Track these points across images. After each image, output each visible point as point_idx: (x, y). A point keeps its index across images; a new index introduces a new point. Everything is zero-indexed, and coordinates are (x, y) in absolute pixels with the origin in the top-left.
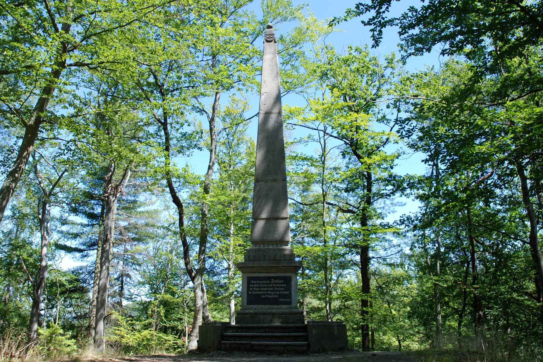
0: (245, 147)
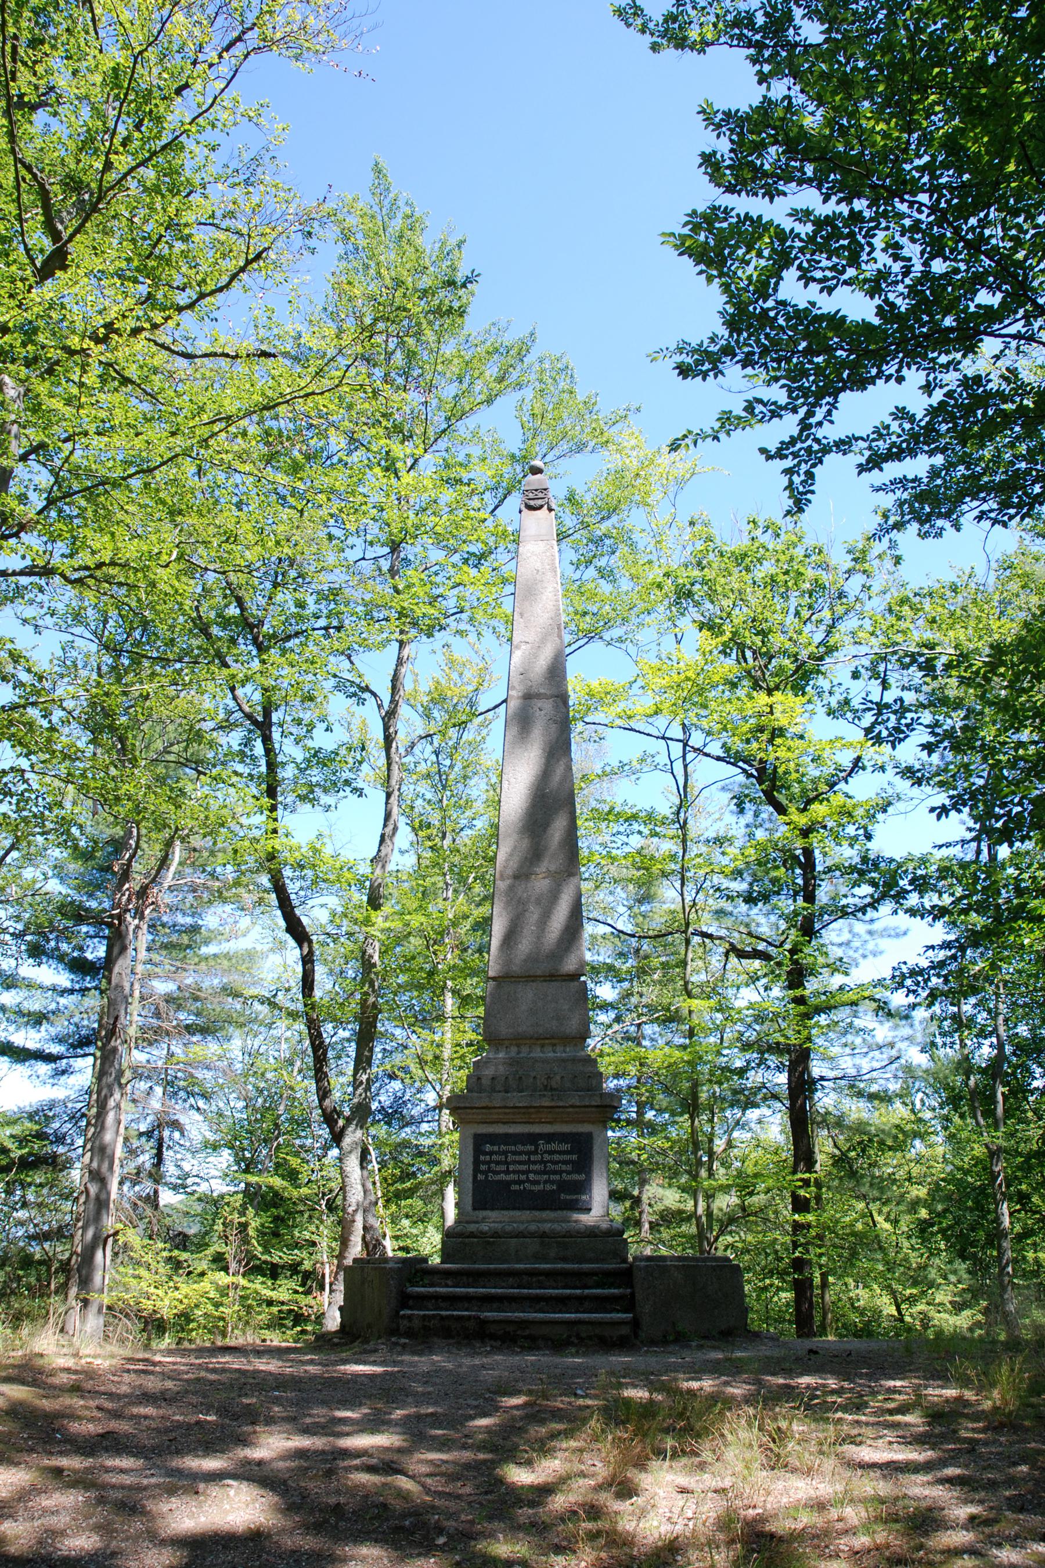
0: (483, 786)
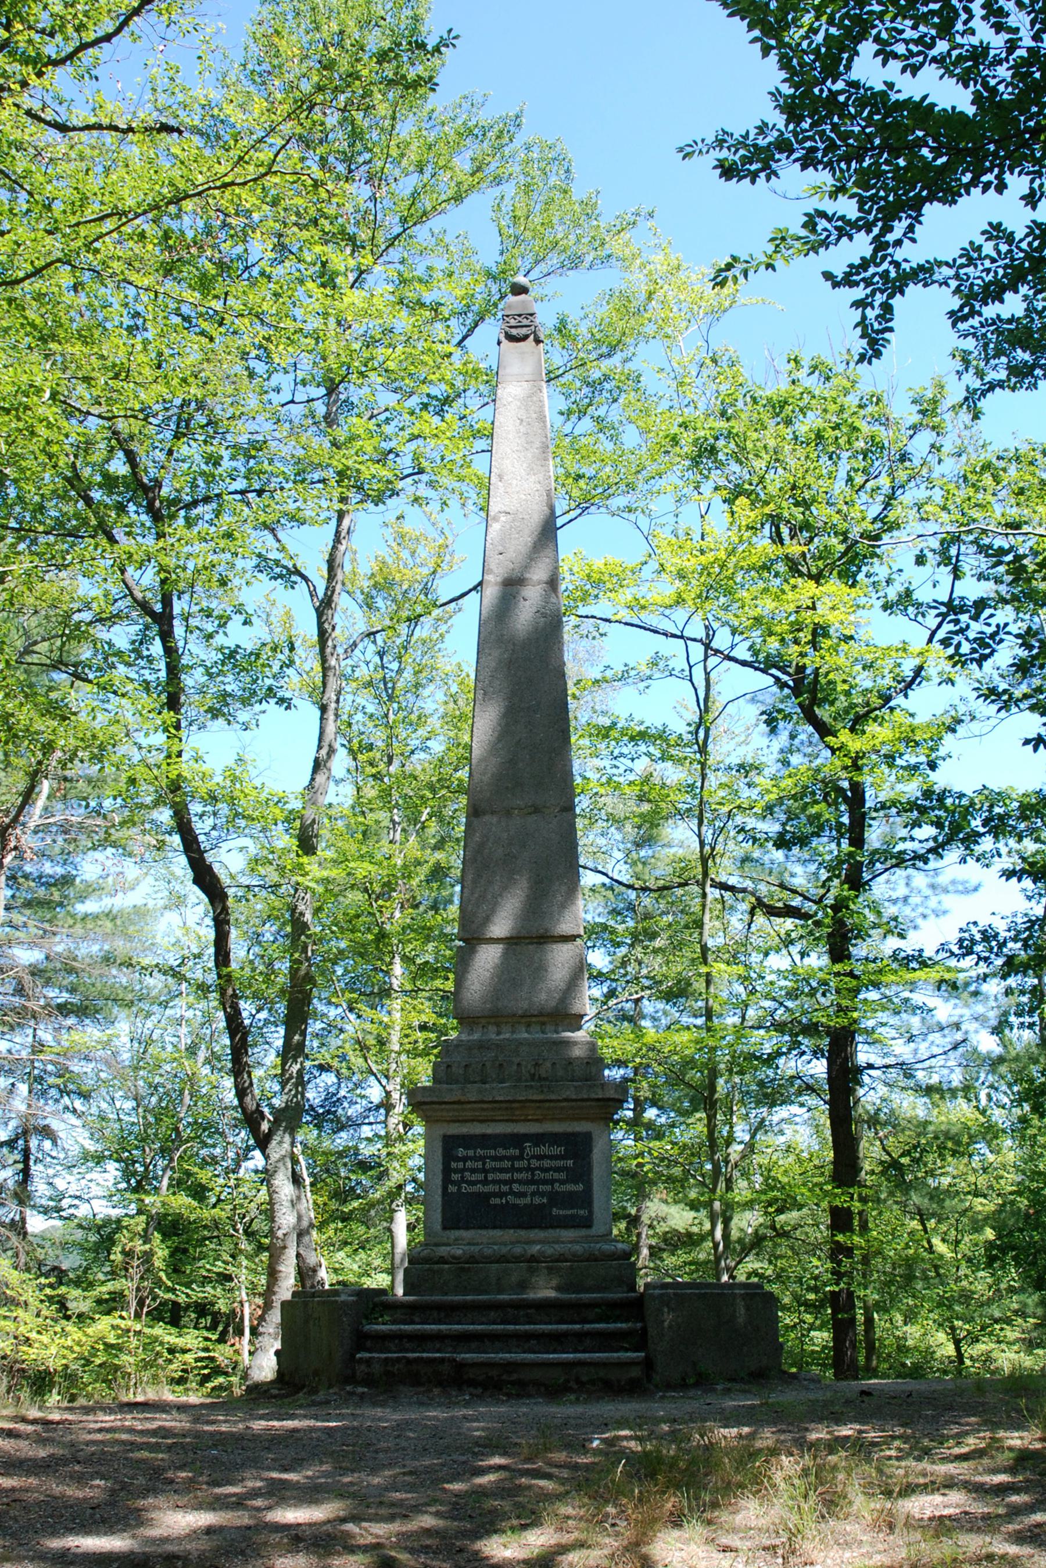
0: (440, 696)
